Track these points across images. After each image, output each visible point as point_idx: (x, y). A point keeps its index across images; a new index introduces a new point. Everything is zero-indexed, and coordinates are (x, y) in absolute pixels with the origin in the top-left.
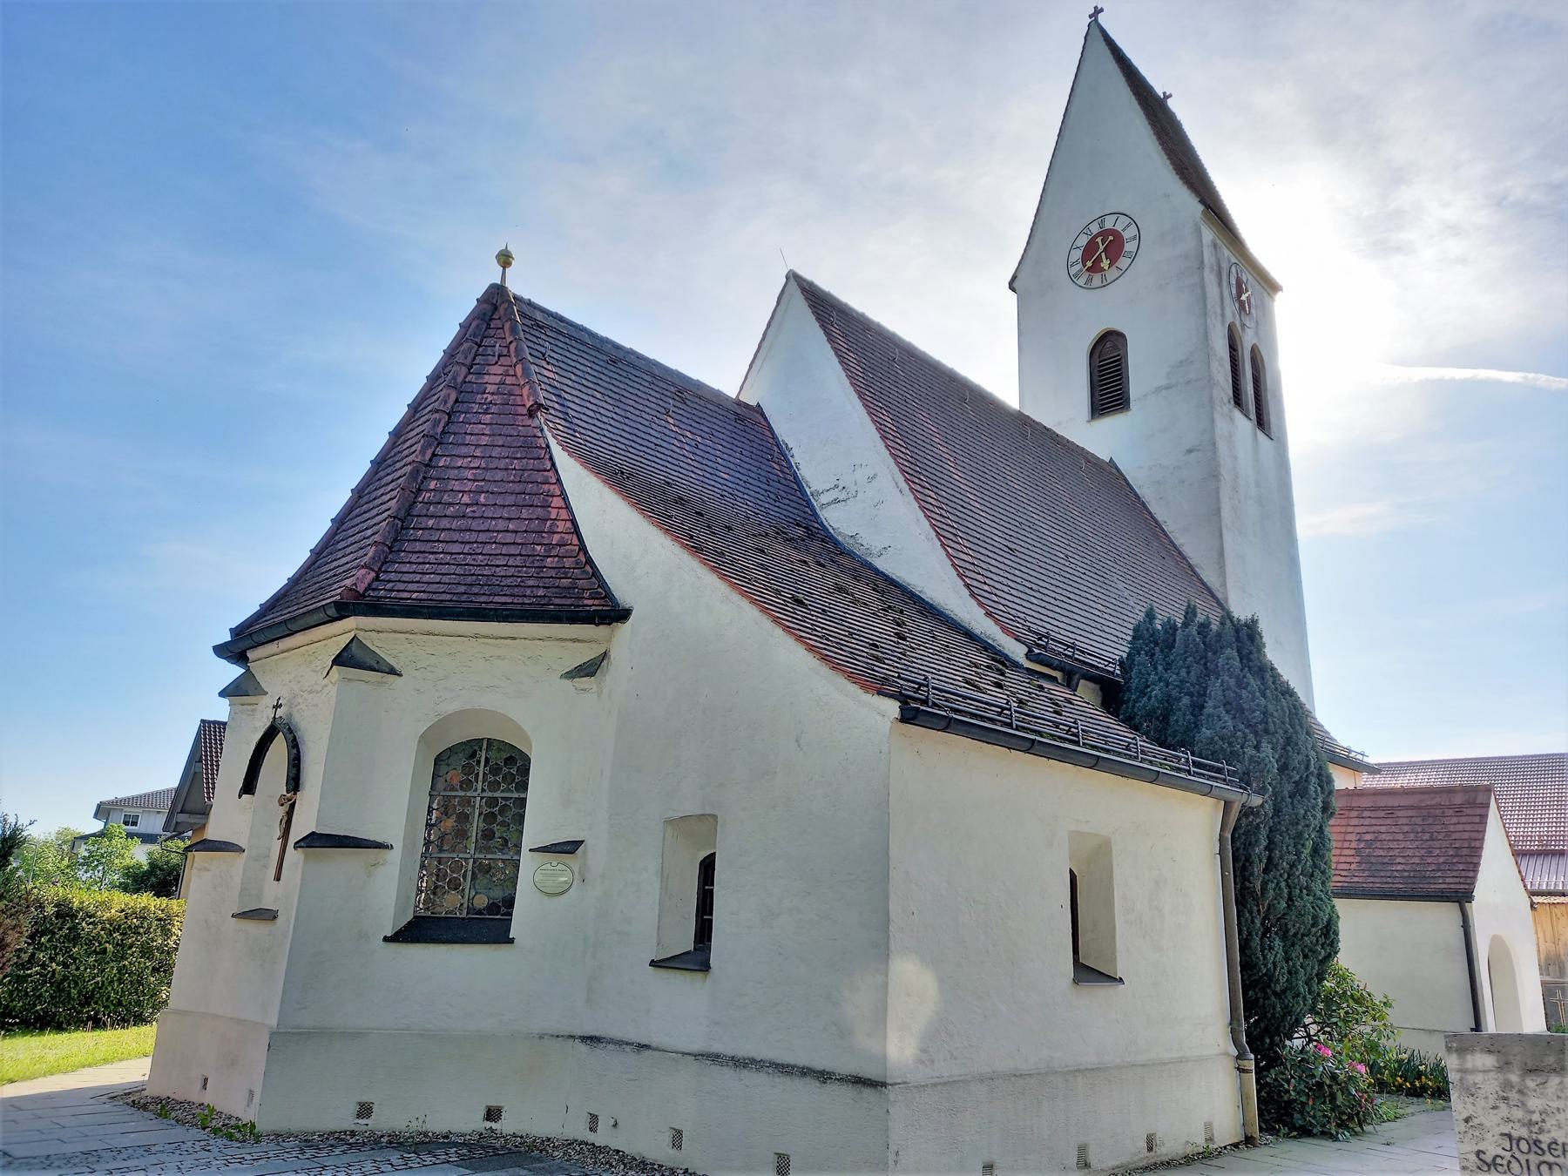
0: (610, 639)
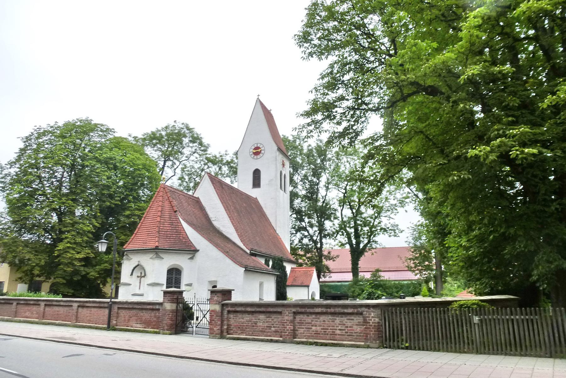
0: (195, 253)
